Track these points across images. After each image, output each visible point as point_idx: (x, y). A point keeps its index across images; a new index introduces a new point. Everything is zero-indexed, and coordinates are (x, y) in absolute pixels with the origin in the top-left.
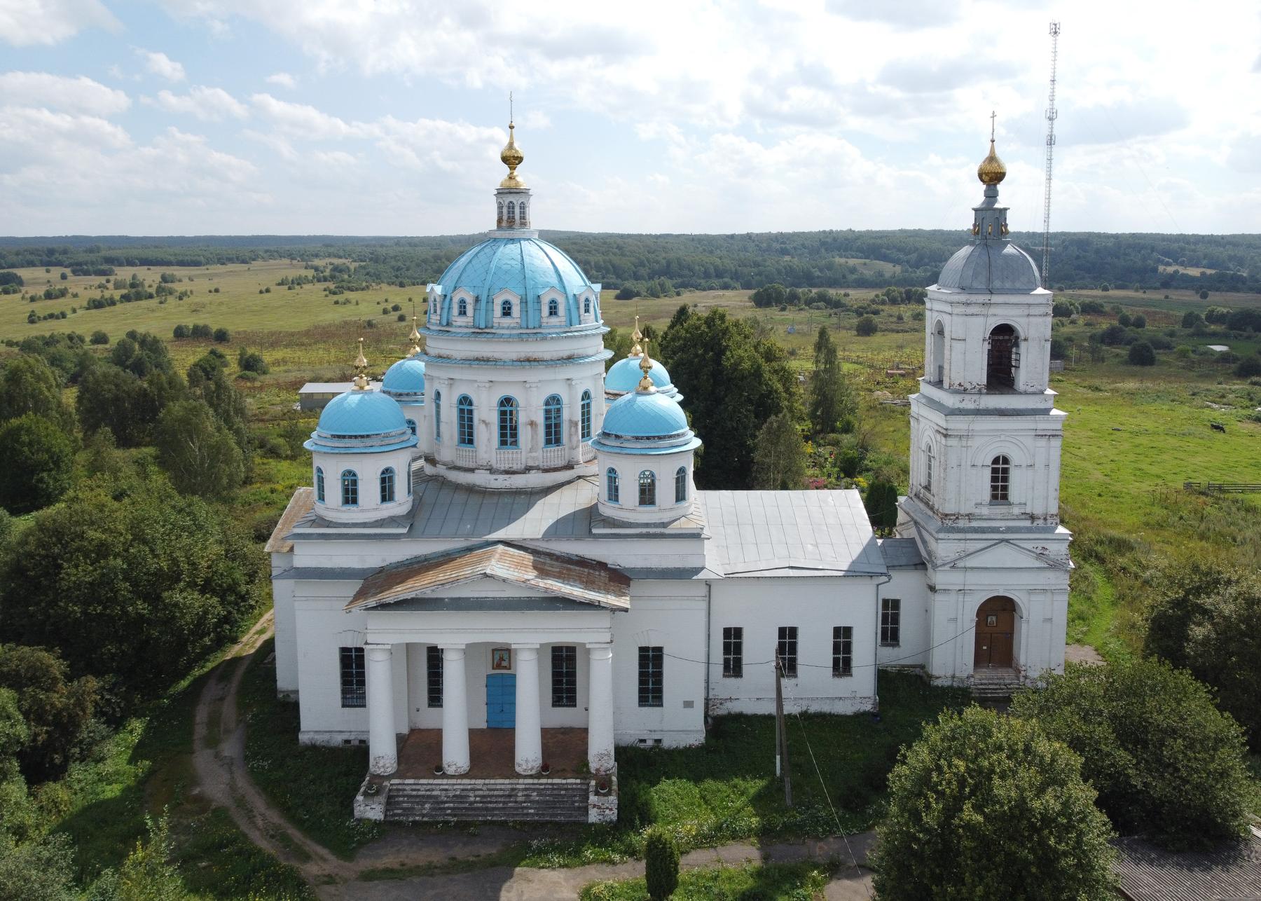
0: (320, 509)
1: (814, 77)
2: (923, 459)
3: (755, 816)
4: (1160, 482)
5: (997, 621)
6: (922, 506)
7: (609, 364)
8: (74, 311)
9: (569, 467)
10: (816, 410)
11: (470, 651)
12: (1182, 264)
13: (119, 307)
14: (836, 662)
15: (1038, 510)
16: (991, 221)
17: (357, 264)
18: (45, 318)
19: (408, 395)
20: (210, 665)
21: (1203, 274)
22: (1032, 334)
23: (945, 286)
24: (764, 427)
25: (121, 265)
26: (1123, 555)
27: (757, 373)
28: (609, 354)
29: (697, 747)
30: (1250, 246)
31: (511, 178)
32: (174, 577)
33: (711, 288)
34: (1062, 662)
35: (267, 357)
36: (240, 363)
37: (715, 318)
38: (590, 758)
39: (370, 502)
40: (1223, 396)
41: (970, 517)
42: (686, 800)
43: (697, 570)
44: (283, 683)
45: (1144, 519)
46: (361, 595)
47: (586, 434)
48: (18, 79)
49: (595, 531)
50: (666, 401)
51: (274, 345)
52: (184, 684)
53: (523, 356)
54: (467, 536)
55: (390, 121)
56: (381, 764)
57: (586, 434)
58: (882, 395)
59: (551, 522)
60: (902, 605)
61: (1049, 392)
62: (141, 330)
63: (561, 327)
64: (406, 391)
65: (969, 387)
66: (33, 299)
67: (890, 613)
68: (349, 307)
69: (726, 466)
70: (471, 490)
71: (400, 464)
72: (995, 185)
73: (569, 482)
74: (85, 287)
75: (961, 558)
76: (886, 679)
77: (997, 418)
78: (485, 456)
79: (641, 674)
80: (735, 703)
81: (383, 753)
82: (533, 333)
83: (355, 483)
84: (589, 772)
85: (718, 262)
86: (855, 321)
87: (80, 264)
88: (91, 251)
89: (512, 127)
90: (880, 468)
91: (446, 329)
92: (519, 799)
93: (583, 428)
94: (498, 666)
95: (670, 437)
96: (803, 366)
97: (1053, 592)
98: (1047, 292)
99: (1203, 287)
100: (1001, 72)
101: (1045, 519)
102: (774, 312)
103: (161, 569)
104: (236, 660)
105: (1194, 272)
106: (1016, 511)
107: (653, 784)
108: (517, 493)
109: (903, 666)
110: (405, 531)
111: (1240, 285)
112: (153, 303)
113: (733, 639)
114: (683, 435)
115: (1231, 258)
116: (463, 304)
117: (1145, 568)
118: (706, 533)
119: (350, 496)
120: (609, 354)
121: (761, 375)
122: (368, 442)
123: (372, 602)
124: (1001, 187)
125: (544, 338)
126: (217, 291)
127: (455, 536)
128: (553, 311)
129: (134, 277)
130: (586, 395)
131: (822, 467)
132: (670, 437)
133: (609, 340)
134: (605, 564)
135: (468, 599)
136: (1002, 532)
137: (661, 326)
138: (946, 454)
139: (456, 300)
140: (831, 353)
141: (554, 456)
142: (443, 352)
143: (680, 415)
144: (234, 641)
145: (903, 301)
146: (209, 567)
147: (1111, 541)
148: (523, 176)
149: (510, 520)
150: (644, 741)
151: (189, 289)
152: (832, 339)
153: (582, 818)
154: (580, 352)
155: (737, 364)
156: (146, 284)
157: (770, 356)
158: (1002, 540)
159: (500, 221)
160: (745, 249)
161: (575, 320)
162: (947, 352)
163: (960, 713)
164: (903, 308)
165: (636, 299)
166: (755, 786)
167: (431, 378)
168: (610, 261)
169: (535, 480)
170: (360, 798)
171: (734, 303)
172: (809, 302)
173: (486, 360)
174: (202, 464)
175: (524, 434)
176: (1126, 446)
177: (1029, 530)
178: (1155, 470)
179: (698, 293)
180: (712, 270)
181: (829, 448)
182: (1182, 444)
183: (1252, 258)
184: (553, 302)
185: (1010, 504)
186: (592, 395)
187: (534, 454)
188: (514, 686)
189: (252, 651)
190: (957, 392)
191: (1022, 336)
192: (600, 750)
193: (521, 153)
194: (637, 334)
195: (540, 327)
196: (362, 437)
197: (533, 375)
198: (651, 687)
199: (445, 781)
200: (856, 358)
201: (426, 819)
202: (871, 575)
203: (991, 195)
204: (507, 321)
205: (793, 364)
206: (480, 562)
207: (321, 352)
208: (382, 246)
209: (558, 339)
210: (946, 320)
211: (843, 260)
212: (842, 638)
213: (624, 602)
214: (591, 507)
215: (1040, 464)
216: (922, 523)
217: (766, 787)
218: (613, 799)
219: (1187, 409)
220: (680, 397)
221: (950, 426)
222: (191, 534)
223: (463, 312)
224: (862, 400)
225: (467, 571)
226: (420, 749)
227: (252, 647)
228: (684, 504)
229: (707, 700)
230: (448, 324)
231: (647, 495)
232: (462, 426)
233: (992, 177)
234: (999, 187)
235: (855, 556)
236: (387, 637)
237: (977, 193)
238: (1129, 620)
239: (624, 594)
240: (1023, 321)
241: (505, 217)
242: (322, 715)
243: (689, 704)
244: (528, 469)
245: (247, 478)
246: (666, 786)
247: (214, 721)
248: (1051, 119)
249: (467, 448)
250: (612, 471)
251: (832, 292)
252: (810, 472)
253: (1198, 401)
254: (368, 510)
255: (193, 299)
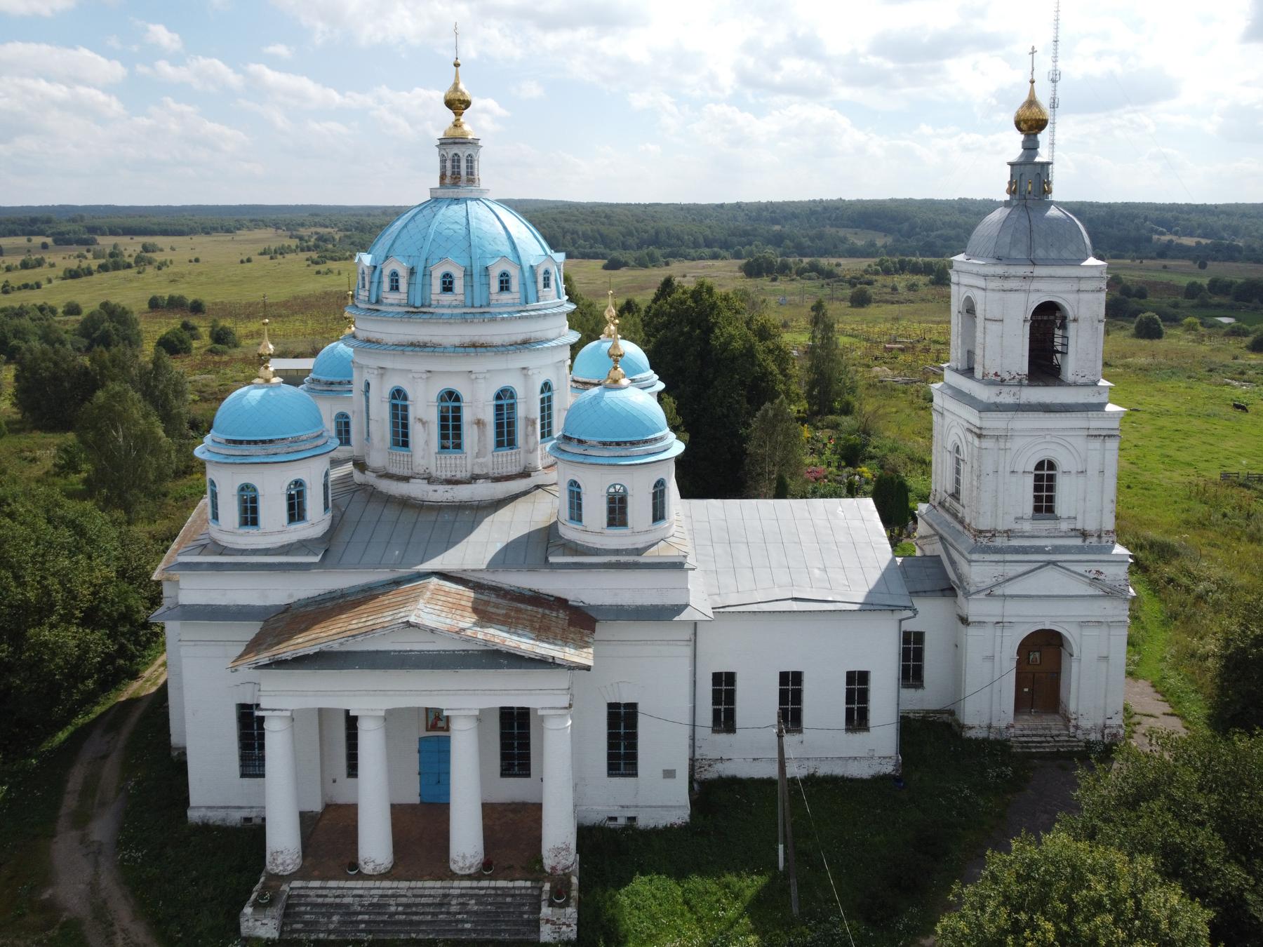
0: (214, 530)
1: (806, 48)
2: (949, 461)
3: (752, 932)
4: (1191, 471)
5: (1042, 659)
6: (948, 517)
7: (575, 349)
8: (50, 281)
9: (525, 474)
10: (812, 389)
11: (391, 717)
12: (1176, 233)
13: (96, 277)
14: (849, 713)
15: (1091, 526)
16: (1030, 180)
17: (342, 234)
18: (19, 289)
19: (340, 383)
20: (98, 710)
21: (1198, 243)
22: (1083, 313)
23: (974, 256)
24: (758, 414)
25: (103, 234)
26: (1167, 563)
27: (749, 353)
28: (574, 337)
29: (680, 827)
30: (1244, 215)
31: (457, 125)
32: (42, 611)
33: (701, 258)
34: (1121, 709)
35: (241, 329)
36: (211, 336)
37: (702, 292)
38: (545, 852)
39: (274, 525)
40: (1242, 373)
41: (1009, 533)
42: (666, 906)
43: (679, 609)
44: (175, 740)
45: (1184, 516)
46: (254, 646)
47: (546, 433)
48: (17, 49)
49: (552, 559)
50: (641, 397)
51: (250, 316)
52: (62, 736)
53: (467, 340)
54: (393, 567)
55: (384, 91)
56: (279, 861)
57: (546, 433)
58: (881, 371)
59: (499, 546)
60: (927, 638)
61: (1103, 383)
62: (114, 300)
63: (514, 305)
64: (338, 379)
65: (1007, 377)
66: (8, 269)
67: (912, 651)
68: (333, 277)
69: (715, 469)
70: (405, 503)
71: (313, 474)
72: (1036, 135)
73: (525, 493)
74: (63, 259)
75: (999, 584)
76: (912, 729)
77: (1041, 414)
78: (422, 462)
79: (611, 736)
80: (727, 764)
81: (283, 843)
82: (479, 312)
83: (254, 500)
84: (542, 870)
85: (708, 232)
86: (848, 292)
87: (62, 234)
88: (74, 220)
89: (457, 65)
90: (885, 456)
91: (375, 307)
92: (453, 909)
93: (543, 427)
94: (434, 727)
95: (646, 442)
96: (796, 339)
97: (1109, 625)
98: (1100, 263)
99: (1201, 258)
100: (988, 43)
101: (1099, 536)
102: (764, 282)
103: (27, 601)
104: (133, 702)
105: (1189, 241)
106: (1064, 526)
107: (623, 881)
108: (459, 507)
109: (928, 712)
110: (316, 559)
111: (1237, 255)
112: (131, 273)
113: (724, 685)
114: (662, 439)
115: (1225, 228)
116: (394, 277)
117: (1196, 579)
118: (690, 561)
119: (250, 515)
120: (574, 337)
121: (753, 356)
122: (271, 448)
123: (264, 658)
124: (1043, 137)
125: (494, 319)
126: (197, 260)
127: (378, 565)
128: (505, 285)
129: (115, 246)
130: (547, 387)
131: (821, 454)
132: (646, 442)
133: (575, 321)
134: (566, 601)
135: (388, 652)
136: (1048, 553)
137: (644, 299)
138: (980, 457)
139: (387, 272)
140: (829, 328)
141: (507, 461)
142: (374, 336)
143: (657, 413)
144: (134, 676)
145: (896, 272)
146: (93, 594)
147: (1152, 545)
148: (471, 124)
149: (450, 543)
150: (614, 819)
151: (169, 258)
152: (829, 313)
153: (532, 937)
154: (539, 335)
155: (727, 343)
156: (126, 254)
157: (764, 333)
158: (1049, 563)
159: (443, 177)
160: (735, 218)
161: (531, 295)
162: (979, 334)
163: (1039, 842)
164: (896, 278)
165: (624, 269)
166: (751, 885)
167: (361, 367)
168: (598, 231)
169: (483, 491)
170: (248, 910)
171: (723, 275)
172: (800, 273)
173: (424, 346)
174: (128, 453)
175: (469, 435)
176: (1148, 429)
177: (1080, 550)
178: (1184, 456)
179: (687, 263)
180: (701, 240)
181: (828, 432)
182: (1208, 426)
183: (1247, 228)
184: (504, 274)
185: (1057, 518)
186: (554, 387)
187: (481, 460)
188: (449, 751)
189: (154, 689)
190: (991, 383)
191: (1071, 315)
192: (558, 839)
193: (468, 95)
194: (610, 313)
195: (489, 305)
196: (264, 442)
197: (480, 364)
198: (622, 748)
199: (360, 884)
200: (854, 330)
201: (332, 937)
202: (893, 609)
203: (1031, 147)
204: (447, 298)
205: (787, 338)
206: (404, 603)
207: (297, 324)
208: (369, 215)
209: (511, 319)
210: (978, 297)
211: (833, 230)
212: (858, 684)
213: (583, 657)
214: (550, 526)
215: (1093, 471)
216: (950, 539)
217: (766, 887)
218: (571, 911)
219: (1204, 386)
220: (661, 386)
221: (986, 424)
222: (72, 554)
223: (395, 288)
224: (861, 377)
225: (387, 617)
226: (329, 833)
227: (154, 684)
228: (663, 524)
229: (693, 761)
230: (378, 302)
231: (617, 511)
232: (395, 425)
233: (1031, 125)
234: (1040, 137)
235: (872, 584)
236: (286, 698)
237: (1013, 144)
238: (1187, 647)
239: (586, 645)
240: (1072, 297)
241: (449, 173)
242: (212, 786)
243: (669, 774)
244: (474, 478)
245: (187, 467)
246: (640, 884)
247: (88, 790)
248: (1054, 81)
249: (402, 451)
250: (574, 483)
251: (824, 262)
252: (808, 460)
253: (1216, 378)
254: (271, 533)
255: (172, 269)
